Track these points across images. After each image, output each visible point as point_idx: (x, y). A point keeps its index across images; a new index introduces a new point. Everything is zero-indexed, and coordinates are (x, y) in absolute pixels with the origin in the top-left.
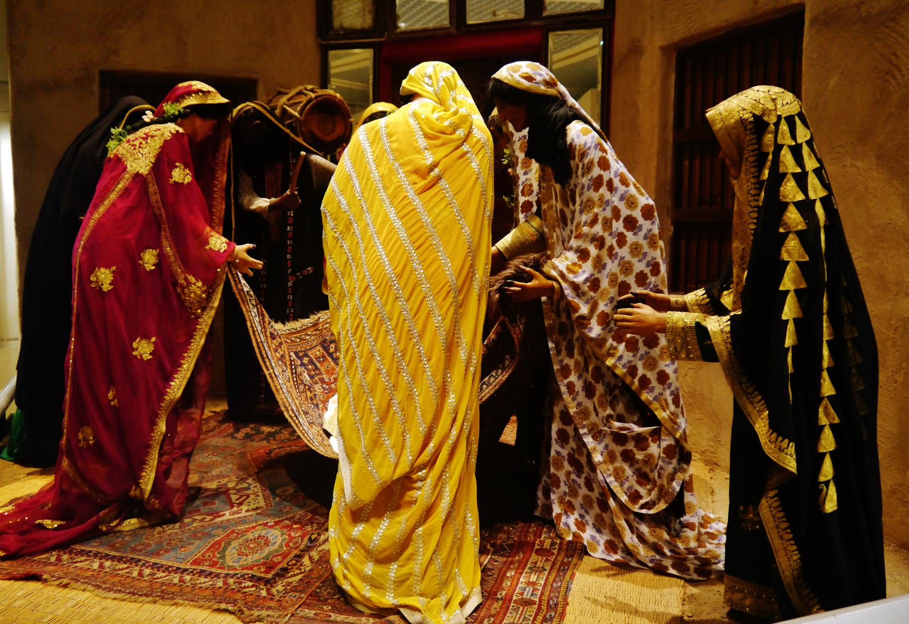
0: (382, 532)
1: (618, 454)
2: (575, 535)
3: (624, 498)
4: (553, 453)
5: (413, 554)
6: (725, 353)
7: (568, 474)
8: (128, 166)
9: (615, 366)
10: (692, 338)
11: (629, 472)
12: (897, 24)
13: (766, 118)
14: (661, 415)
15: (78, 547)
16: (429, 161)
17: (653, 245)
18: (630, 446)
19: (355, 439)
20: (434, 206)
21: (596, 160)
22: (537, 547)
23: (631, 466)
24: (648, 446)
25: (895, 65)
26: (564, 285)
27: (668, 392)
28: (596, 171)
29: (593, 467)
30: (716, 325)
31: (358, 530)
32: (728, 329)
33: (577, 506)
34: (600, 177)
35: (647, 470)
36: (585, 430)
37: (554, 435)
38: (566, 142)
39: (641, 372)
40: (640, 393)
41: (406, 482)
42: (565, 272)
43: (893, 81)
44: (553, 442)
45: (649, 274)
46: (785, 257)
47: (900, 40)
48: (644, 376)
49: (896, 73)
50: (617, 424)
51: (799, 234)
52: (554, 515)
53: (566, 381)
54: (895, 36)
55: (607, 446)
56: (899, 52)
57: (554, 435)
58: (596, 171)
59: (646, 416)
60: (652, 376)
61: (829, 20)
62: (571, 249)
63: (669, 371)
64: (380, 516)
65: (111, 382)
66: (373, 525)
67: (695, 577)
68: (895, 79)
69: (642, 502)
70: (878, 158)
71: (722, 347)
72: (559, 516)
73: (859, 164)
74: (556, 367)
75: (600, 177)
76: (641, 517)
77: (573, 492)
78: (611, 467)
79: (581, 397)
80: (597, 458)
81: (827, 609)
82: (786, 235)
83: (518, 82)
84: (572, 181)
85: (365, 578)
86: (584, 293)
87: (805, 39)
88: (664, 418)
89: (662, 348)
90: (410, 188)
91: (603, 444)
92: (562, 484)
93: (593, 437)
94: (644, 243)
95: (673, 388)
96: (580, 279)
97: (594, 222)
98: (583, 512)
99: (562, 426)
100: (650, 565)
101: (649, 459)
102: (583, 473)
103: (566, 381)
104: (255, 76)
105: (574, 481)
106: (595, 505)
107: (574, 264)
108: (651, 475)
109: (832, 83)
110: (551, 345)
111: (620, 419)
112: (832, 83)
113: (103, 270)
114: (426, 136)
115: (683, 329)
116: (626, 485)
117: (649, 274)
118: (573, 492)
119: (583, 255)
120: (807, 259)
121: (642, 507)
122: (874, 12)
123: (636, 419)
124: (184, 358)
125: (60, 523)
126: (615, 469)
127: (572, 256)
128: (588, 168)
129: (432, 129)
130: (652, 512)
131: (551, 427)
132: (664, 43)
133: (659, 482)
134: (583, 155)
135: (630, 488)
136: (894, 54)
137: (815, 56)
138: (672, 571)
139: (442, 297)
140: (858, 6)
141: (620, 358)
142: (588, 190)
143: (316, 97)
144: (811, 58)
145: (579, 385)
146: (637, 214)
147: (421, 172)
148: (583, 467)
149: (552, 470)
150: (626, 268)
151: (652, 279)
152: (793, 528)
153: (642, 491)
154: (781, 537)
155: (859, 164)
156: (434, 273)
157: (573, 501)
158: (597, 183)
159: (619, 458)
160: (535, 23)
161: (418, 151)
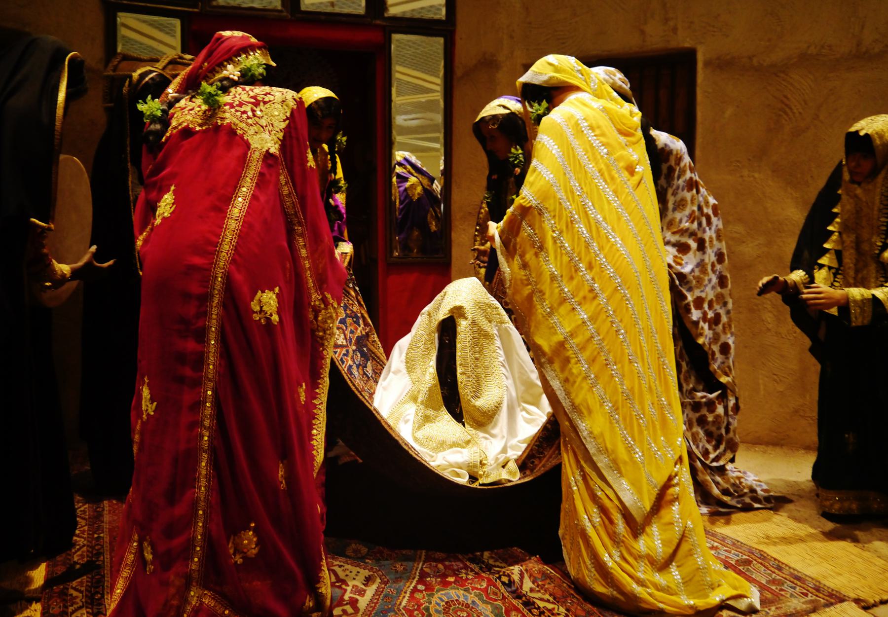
1: (694, 420)
10: (868, 309)
11: (701, 434)
12: (787, 75)
14: (724, 379)
18: (704, 411)
23: (702, 429)
24: (716, 408)
25: (786, 105)
28: (688, 175)
38: (656, 146)
42: (673, 264)
43: (785, 116)
49: (787, 110)
56: (789, 96)
58: (688, 175)
61: (723, 65)
63: (730, 342)
69: (712, 456)
70: (773, 171)
73: (756, 175)
88: (729, 382)
89: (724, 325)
100: (739, 506)
107: (675, 257)
115: (862, 301)
121: (714, 460)
128: (682, 172)
134: (679, 159)
136: (786, 97)
138: (756, 505)
140: (750, 58)
142: (683, 190)
153: (710, 447)
155: (756, 175)
159: (695, 424)
160: (378, 22)
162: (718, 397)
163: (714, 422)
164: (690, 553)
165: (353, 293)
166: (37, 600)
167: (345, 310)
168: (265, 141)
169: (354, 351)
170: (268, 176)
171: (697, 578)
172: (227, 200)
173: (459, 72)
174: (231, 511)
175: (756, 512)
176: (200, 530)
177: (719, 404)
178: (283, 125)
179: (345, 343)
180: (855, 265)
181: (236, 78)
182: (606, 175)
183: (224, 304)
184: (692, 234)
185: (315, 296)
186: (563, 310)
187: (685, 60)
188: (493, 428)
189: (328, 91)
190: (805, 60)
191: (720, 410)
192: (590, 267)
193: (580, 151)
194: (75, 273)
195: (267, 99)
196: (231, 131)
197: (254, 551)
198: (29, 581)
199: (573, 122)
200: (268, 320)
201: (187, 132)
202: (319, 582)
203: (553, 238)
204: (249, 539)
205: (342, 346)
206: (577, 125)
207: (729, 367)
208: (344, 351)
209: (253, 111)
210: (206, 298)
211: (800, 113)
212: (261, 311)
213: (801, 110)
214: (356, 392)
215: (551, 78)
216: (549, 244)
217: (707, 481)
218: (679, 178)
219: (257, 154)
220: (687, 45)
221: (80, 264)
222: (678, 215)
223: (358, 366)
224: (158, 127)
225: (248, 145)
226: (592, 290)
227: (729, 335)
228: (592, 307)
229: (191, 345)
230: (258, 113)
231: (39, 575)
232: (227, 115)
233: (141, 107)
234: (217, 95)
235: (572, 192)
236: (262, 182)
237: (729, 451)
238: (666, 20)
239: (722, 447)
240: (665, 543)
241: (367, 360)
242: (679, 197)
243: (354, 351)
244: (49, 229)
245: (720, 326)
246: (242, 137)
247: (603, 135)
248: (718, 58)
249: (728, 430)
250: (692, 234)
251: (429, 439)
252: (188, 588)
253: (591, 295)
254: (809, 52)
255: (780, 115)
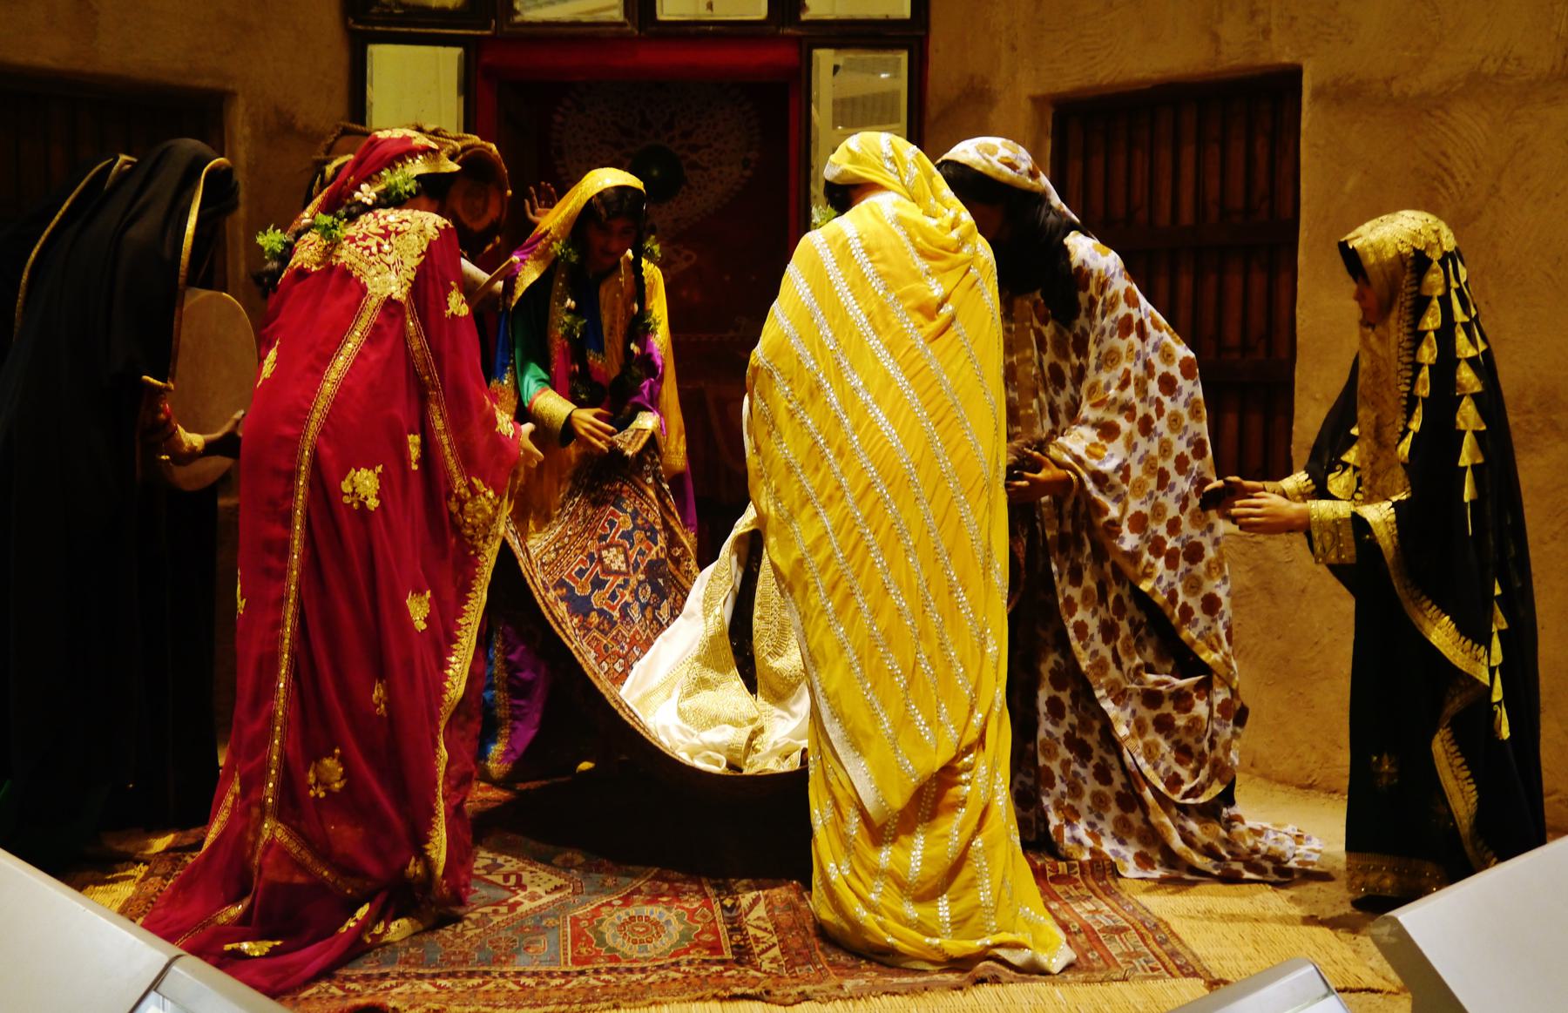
0: (916, 855)
1: (1149, 722)
2: (1092, 851)
3: (1162, 787)
4: (1041, 735)
5: (973, 879)
6: (1391, 548)
7: (1065, 764)
8: (369, 286)
9: (1153, 590)
10: (1347, 534)
11: (1165, 746)
12: (1447, 113)
13: (1428, 254)
14: (1208, 657)
15: (346, 972)
16: (937, 292)
17: (1195, 414)
18: (1167, 708)
19: (866, 719)
20: (951, 362)
21: (1122, 293)
22: (1049, 874)
23: (1167, 738)
24: (1192, 705)
25: (1445, 170)
26: (1085, 476)
27: (1220, 624)
28: (1122, 309)
29: (1114, 745)
30: (1379, 514)
31: (885, 857)
32: (1393, 518)
33: (1084, 810)
34: (1129, 317)
35: (1190, 740)
36: (1103, 692)
37: (1042, 707)
38: (1070, 264)
39: (1181, 598)
40: (1181, 630)
41: (947, 775)
42: (1084, 456)
43: (1442, 190)
44: (1042, 718)
45: (1190, 457)
46: (1462, 426)
47: (1451, 135)
48: (1184, 604)
49: (1447, 179)
50: (1152, 677)
51: (1474, 396)
52: (1051, 828)
53: (1072, 621)
54: (1443, 128)
55: (1134, 712)
56: (1450, 151)
57: (1042, 707)
58: (1122, 309)
59: (1186, 662)
60: (1195, 603)
62: (1085, 422)
63: (1221, 593)
64: (910, 831)
65: (380, 671)
66: (902, 846)
67: (1275, 878)
68: (1447, 188)
69: (1185, 788)
71: (1388, 542)
72: (1059, 829)
74: (1061, 601)
75: (1129, 317)
76: (1184, 809)
77: (1075, 790)
78: (1140, 743)
79: (1097, 642)
80: (1122, 731)
81: (1503, 857)
82: (1461, 397)
83: (1000, 172)
84: (1082, 321)
85: (908, 923)
86: (1112, 488)
87: (1303, 115)
90: (916, 330)
91: (1129, 710)
92: (1058, 781)
93: (1114, 701)
94: (1184, 412)
95: (1225, 619)
96: (1108, 466)
97: (1124, 384)
98: (1093, 818)
99: (1053, 692)
100: (1216, 872)
101: (1194, 725)
102: (1089, 758)
103: (1072, 621)
104: (230, 87)
105: (1076, 774)
106: (1113, 805)
107: (1094, 445)
108: (1196, 748)
109: (1350, 184)
110: (1054, 568)
111: (1150, 669)
112: (1350, 184)
113: (364, 472)
114: (923, 254)
115: (1334, 521)
116: (1162, 768)
117: (1190, 457)
118: (1075, 790)
119: (1108, 431)
120: (1484, 428)
121: (1186, 796)
122: (1411, 94)
123: (1170, 668)
124: (459, 627)
125: (270, 944)
126: (1146, 745)
127: (1090, 434)
128: (1111, 305)
129: (931, 243)
130: (1201, 800)
131: (1036, 696)
132: (1039, 92)
133: (1211, 756)
134: (1103, 285)
135: (1168, 769)
136: (1444, 154)
137: (1321, 142)
138: (1247, 875)
139: (976, 496)
140: (1388, 82)
141: (1160, 579)
142: (1111, 336)
143: (464, 149)
144: (1315, 145)
145: (1093, 625)
146: (1175, 371)
147: (929, 310)
148: (1091, 750)
149: (1042, 761)
150: (1165, 449)
151: (1195, 464)
152: (1470, 764)
153: (1184, 773)
154: (1456, 778)
156: (964, 459)
157: (1076, 804)
158: (1125, 326)
159: (1151, 728)
160: (788, 31)
161: (916, 276)
162: (1197, 686)
163: (1188, 729)
164: (972, 884)
165: (651, 493)
166: (146, 863)
167: (634, 519)
168: (388, 281)
169: (640, 583)
170: (386, 328)
171: (974, 920)
172: (326, 359)
173: (933, 110)
174: (313, 736)
175: (1245, 887)
176: (276, 750)
177: (1200, 697)
178: (417, 262)
179: (624, 568)
180: (1372, 464)
181: (369, 202)
182: (878, 319)
183: (311, 484)
184: (1127, 409)
185: (459, 484)
186: (807, 512)
187: (1281, 87)
188: (795, 703)
189: (620, 172)
190: (1476, 85)
191: (1201, 708)
192: (840, 453)
193: (842, 287)
194: (211, 448)
195: (401, 229)
196: (345, 274)
197: (337, 785)
198: (150, 846)
199: (840, 242)
200: (362, 504)
201: (302, 273)
202: (427, 842)
203: (790, 411)
204: (332, 766)
205: (618, 573)
206: (845, 246)
207: (1218, 637)
208: (620, 580)
209: (379, 245)
210: (292, 475)
211: (1468, 184)
212: (353, 493)
213: (1469, 179)
214: (552, 622)
215: (844, 172)
216: (782, 418)
217: (1163, 824)
218: (1103, 315)
219: (375, 300)
220: (1286, 60)
221: (219, 434)
222: (1104, 377)
223: (643, 608)
224: (275, 265)
225: (363, 290)
226: (839, 487)
227: (1218, 581)
228: (836, 510)
229: (277, 531)
230: (386, 248)
231: (160, 844)
232: (344, 253)
233: (260, 240)
234: (335, 227)
235: (821, 345)
236: (375, 335)
237: (1216, 781)
238: (1253, 14)
239: (1204, 773)
240: (926, 861)
241: (664, 597)
242: (1105, 347)
243: (640, 583)
244: (168, 389)
245: (1202, 566)
246: (358, 280)
247: (883, 260)
248: (1336, 83)
249: (1212, 745)
250: (1127, 409)
251: (698, 712)
252: (262, 821)
253: (839, 494)
254: (1485, 70)
255: (1435, 189)
